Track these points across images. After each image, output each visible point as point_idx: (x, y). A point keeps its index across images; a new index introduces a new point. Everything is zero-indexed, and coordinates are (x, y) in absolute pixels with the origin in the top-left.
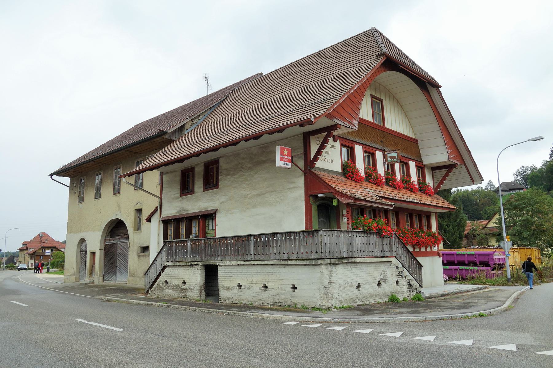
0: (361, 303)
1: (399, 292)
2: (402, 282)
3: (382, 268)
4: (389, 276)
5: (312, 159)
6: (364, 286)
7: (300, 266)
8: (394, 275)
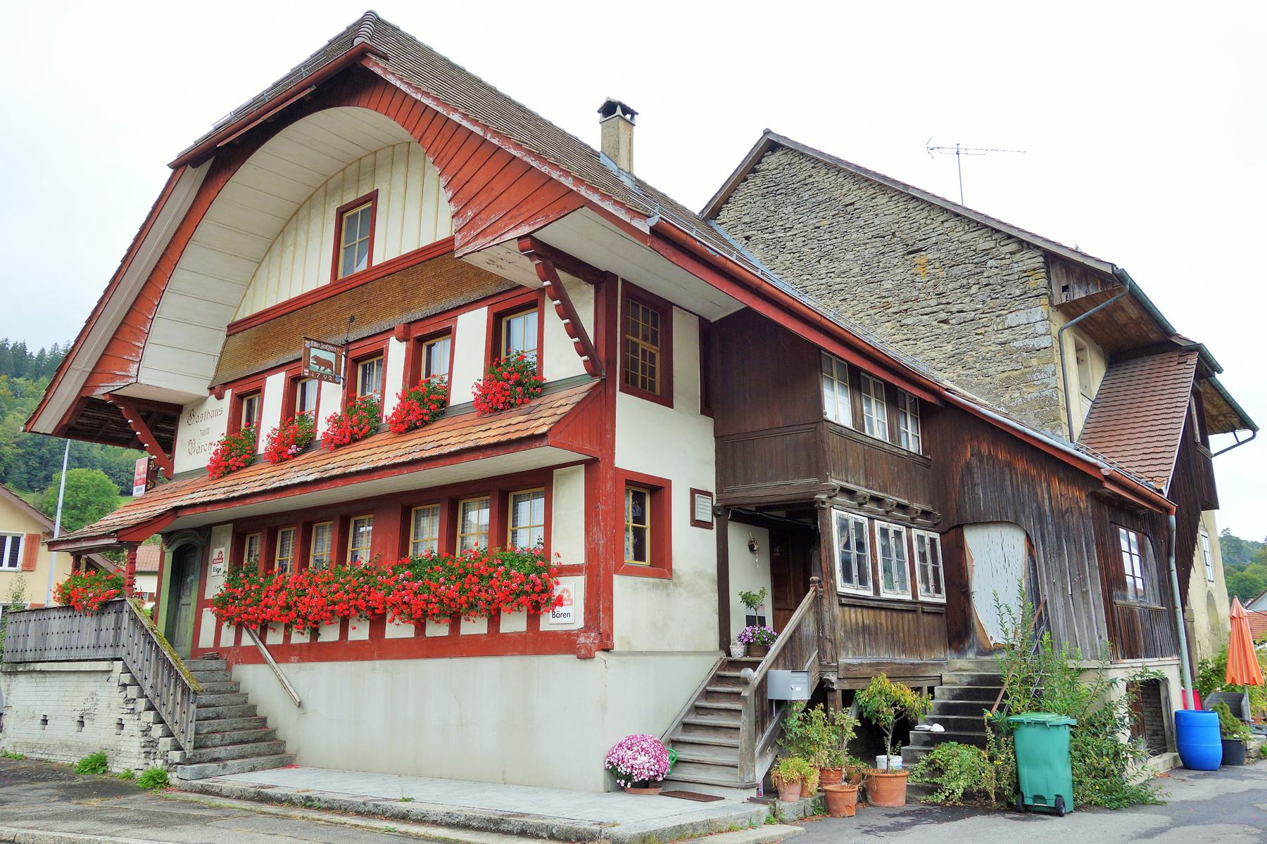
1: (119, 752)
2: (132, 726)
3: (89, 685)
4: (102, 706)
7: (82, 675)
8: (113, 706)
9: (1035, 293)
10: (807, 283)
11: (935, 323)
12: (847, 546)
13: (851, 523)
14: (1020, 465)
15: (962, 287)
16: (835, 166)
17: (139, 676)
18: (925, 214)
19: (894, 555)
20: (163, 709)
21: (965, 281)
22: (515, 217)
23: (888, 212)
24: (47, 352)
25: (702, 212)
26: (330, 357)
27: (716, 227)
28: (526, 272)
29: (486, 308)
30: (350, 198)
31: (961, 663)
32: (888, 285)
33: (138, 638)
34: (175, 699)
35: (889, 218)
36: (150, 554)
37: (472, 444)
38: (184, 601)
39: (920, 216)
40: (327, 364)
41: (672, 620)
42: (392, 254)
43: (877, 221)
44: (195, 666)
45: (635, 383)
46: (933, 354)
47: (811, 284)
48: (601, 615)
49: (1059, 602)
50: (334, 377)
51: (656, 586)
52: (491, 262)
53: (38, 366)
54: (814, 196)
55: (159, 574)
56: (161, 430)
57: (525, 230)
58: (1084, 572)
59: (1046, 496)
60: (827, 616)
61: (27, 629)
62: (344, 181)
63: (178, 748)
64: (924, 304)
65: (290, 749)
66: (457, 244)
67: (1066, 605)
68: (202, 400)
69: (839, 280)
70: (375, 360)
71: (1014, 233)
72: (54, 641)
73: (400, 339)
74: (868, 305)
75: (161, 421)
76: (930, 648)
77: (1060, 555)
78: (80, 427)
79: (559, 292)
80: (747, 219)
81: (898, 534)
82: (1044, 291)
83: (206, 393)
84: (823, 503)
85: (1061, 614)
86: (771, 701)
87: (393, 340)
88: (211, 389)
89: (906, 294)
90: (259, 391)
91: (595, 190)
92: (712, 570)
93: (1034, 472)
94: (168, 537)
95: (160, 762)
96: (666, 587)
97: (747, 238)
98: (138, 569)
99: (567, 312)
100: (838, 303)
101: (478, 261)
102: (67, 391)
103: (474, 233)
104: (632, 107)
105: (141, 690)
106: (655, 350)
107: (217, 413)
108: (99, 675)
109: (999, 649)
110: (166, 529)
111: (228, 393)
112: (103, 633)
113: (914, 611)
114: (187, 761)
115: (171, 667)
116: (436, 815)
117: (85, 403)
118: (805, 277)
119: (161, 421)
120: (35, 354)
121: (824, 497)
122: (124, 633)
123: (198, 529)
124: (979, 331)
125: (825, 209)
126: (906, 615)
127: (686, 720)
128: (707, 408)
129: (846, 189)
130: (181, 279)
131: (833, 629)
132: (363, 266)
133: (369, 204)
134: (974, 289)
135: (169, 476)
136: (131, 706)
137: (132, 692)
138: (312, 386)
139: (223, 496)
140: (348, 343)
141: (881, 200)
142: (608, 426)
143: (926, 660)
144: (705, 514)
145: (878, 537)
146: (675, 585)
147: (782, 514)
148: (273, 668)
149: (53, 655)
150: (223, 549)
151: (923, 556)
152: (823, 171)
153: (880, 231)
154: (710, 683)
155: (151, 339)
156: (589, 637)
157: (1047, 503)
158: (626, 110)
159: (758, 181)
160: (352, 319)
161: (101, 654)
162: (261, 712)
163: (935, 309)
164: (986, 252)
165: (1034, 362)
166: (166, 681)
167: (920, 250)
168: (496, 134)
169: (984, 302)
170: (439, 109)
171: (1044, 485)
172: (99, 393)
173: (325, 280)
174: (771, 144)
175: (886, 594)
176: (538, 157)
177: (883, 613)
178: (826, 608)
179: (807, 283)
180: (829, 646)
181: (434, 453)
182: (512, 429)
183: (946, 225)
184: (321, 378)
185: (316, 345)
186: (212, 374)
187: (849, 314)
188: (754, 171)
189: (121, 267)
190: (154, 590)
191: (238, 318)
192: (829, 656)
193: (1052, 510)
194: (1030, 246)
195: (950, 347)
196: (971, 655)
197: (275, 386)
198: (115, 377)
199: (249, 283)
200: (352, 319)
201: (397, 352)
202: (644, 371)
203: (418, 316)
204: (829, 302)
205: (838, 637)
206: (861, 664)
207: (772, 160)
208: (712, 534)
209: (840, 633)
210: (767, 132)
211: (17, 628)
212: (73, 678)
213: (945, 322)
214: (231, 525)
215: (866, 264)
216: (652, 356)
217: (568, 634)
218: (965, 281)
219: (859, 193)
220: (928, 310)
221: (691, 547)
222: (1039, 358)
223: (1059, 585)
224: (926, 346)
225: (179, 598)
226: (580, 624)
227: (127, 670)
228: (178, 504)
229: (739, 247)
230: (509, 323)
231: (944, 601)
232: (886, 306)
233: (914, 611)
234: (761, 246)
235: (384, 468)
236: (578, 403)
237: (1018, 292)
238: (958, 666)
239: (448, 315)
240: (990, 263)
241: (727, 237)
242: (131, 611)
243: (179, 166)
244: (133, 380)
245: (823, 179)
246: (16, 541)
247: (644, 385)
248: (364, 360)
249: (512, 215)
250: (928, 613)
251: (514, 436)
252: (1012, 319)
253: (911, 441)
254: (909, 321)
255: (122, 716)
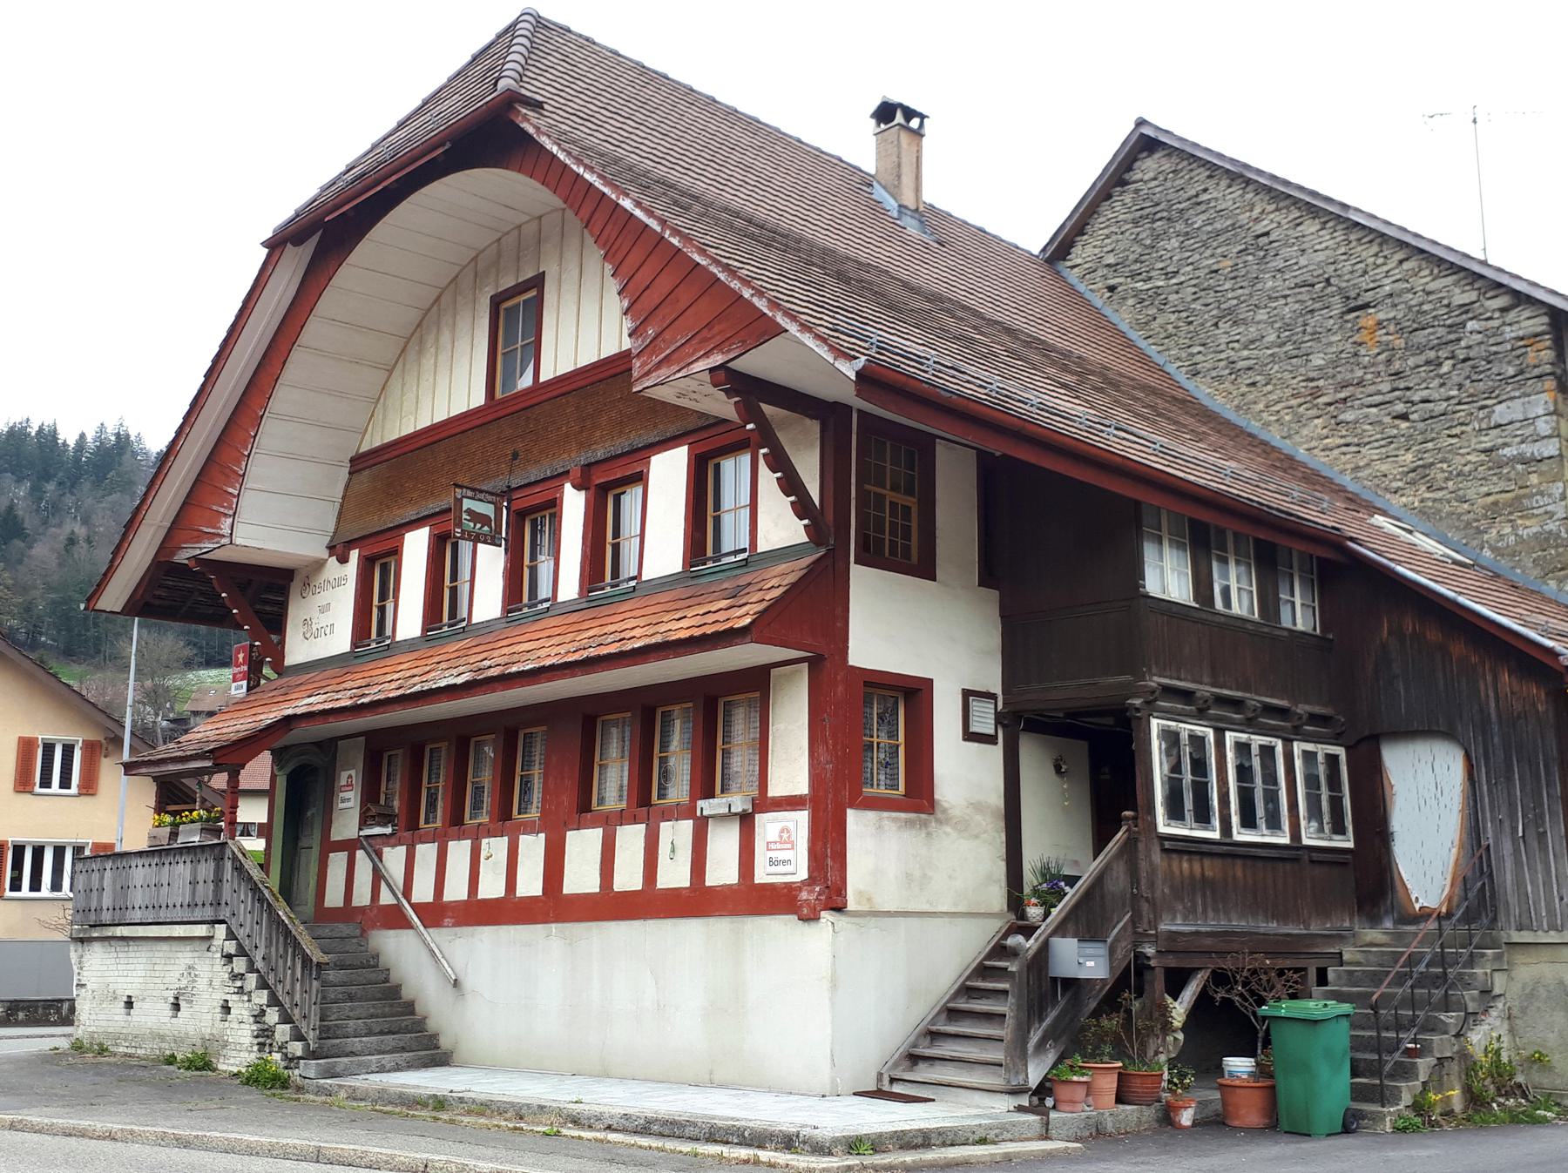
0: (130, 1051)
1: (225, 1045)
2: (241, 1010)
3: (185, 956)
4: (202, 984)
5: (817, 502)
6: (146, 1006)
7: (174, 943)
8: (216, 983)
9: (1536, 372)
10: (1199, 358)
11: (1387, 420)
12: (1176, 768)
13: (1184, 737)
14: (1458, 649)
15: (1428, 363)
16: (1239, 176)
17: (246, 943)
18: (1375, 249)
19: (1258, 780)
20: (280, 987)
21: (1432, 354)
22: (706, 340)
23: (1321, 242)
24: (89, 438)
25: (1044, 250)
26: (486, 509)
27: (1066, 273)
28: (723, 406)
29: (685, 449)
30: (508, 282)
31: (1372, 935)
32: (1318, 360)
33: (244, 893)
34: (293, 974)
35: (1321, 256)
36: (258, 771)
37: (658, 639)
38: (304, 842)
39: (1368, 252)
40: (484, 519)
41: (937, 874)
42: (565, 367)
43: (1303, 261)
44: (320, 932)
45: (880, 551)
46: (1384, 468)
47: (1205, 361)
48: (829, 862)
49: (1507, 847)
50: (493, 538)
51: (910, 824)
52: (681, 395)
53: (77, 460)
54: (1210, 222)
55: (269, 794)
56: (267, 602)
57: (717, 359)
58: (1542, 805)
59: (1491, 694)
60: (1143, 865)
61: (102, 879)
62: (499, 255)
63: (298, 1036)
64: (1372, 389)
65: (445, 1042)
66: (635, 374)
67: (1516, 852)
68: (319, 565)
69: (1245, 353)
70: (547, 513)
71: (1505, 280)
72: (138, 898)
73: (577, 487)
74: (1288, 392)
75: (265, 594)
76: (1324, 912)
77: (1509, 779)
78: (157, 602)
79: (766, 435)
80: (1111, 259)
81: (1268, 752)
82: (1548, 369)
83: (324, 554)
84: (1138, 710)
85: (1509, 864)
86: (1054, 980)
87: (568, 487)
88: (331, 548)
89: (1344, 374)
90: (396, 552)
91: (794, 319)
92: (996, 799)
93: (1474, 659)
94: (279, 756)
95: (277, 1056)
96: (925, 824)
97: (1112, 289)
98: (243, 785)
99: (780, 462)
100: (1244, 389)
101: (665, 394)
102: (139, 555)
103: (656, 360)
104: (919, 109)
105: (251, 963)
106: (911, 502)
107: (340, 582)
108: (197, 943)
109: (1425, 914)
110: (277, 745)
111: (354, 555)
112: (200, 886)
113: (1296, 860)
114: (311, 1055)
115: (287, 933)
116: (612, 1117)
117: (162, 568)
118: (1195, 349)
119: (265, 594)
120: (72, 443)
121: (1137, 702)
122: (226, 888)
123: (319, 744)
124: (1454, 431)
125: (1227, 243)
126: (1280, 865)
127: (951, 1005)
128: (988, 577)
129: (1257, 210)
130: (284, 398)
131: (1152, 885)
132: (526, 381)
133: (533, 293)
134: (1445, 368)
135: (279, 668)
136: (239, 984)
137: (240, 965)
138: (465, 547)
139: (349, 703)
140: (510, 490)
141: (1310, 227)
142: (839, 611)
143: (1315, 928)
144: (984, 721)
145: (1230, 755)
146: (939, 822)
147: (1109, 721)
148: (420, 935)
149: (137, 916)
150: (353, 772)
151: (1312, 781)
152: (1224, 183)
153: (1307, 277)
154: (989, 956)
155: (249, 482)
156: (812, 891)
157: (1492, 705)
158: (910, 114)
159: (1128, 198)
160: (515, 456)
161: (198, 914)
162: (407, 994)
163: (1388, 397)
164: (1465, 308)
165: (1534, 479)
166: (281, 951)
167: (1366, 306)
168: (676, 232)
169: (1460, 386)
170: (606, 190)
171: (1489, 678)
172: (182, 557)
173: (478, 399)
174: (1145, 142)
175: (1241, 835)
176: (726, 268)
177: (1239, 862)
178: (1141, 856)
179: (1199, 358)
180: (1145, 907)
181: (613, 649)
182: (710, 618)
183: (1406, 266)
184: (477, 539)
185: (470, 493)
186: (331, 527)
187: (1261, 406)
188: (1123, 183)
189: (203, 385)
190: (264, 820)
191: (365, 448)
192: (1145, 920)
193: (1499, 716)
194: (1530, 300)
195: (1409, 457)
196: (1388, 924)
197: (416, 545)
198: (201, 536)
199: (377, 399)
200: (515, 456)
201: (574, 503)
202: (893, 532)
203: (600, 455)
204: (1231, 388)
205: (1158, 894)
206: (1197, 933)
207: (1149, 166)
208: (996, 753)
209: (1163, 889)
210: (1141, 122)
211: (89, 879)
212: (165, 947)
213: (1404, 417)
214: (362, 739)
215: (1287, 327)
216: (907, 510)
217: (789, 886)
218: (1432, 354)
219: (1276, 216)
220: (1378, 399)
221: (964, 770)
222: (1541, 474)
223: (1507, 824)
224: (1374, 454)
225: (296, 839)
226: (803, 874)
227: (231, 935)
228: (290, 712)
229: (1098, 303)
230: (717, 468)
231: (1350, 845)
232: (1316, 393)
233: (1296, 860)
234: (1131, 302)
235: (553, 667)
236: (794, 585)
237: (1511, 371)
238: (1368, 939)
239: (638, 456)
240: (1471, 325)
241: (1082, 288)
242: (235, 858)
243: (276, 245)
244: (224, 541)
245: (1225, 196)
246: (68, 750)
247: (893, 552)
248: (528, 523)
249: (702, 340)
250: (1320, 862)
251: (709, 630)
252: (1501, 413)
253: (1300, 613)
254: (1349, 416)
255: (228, 997)
